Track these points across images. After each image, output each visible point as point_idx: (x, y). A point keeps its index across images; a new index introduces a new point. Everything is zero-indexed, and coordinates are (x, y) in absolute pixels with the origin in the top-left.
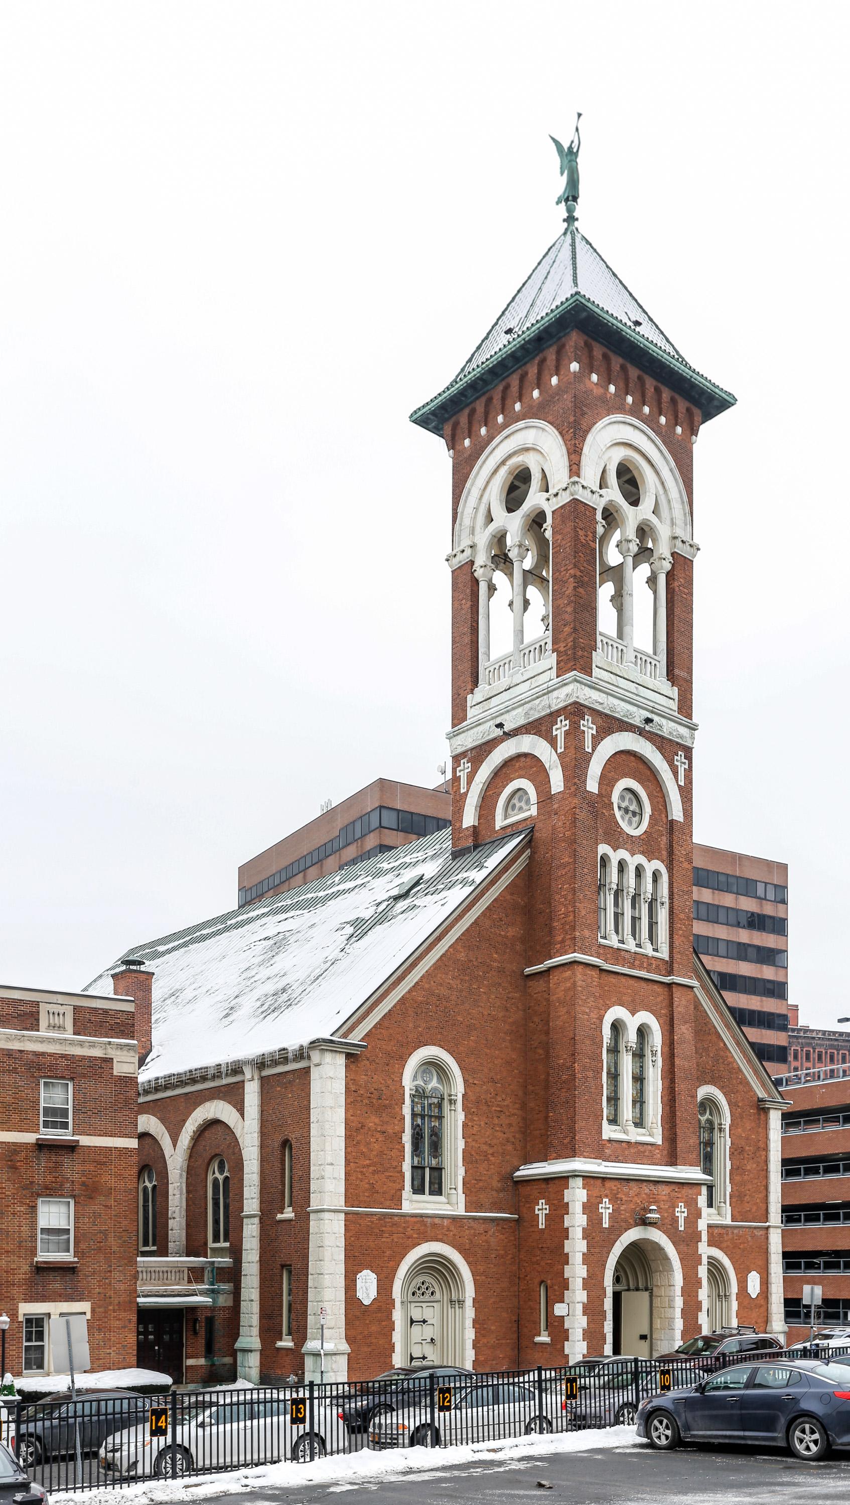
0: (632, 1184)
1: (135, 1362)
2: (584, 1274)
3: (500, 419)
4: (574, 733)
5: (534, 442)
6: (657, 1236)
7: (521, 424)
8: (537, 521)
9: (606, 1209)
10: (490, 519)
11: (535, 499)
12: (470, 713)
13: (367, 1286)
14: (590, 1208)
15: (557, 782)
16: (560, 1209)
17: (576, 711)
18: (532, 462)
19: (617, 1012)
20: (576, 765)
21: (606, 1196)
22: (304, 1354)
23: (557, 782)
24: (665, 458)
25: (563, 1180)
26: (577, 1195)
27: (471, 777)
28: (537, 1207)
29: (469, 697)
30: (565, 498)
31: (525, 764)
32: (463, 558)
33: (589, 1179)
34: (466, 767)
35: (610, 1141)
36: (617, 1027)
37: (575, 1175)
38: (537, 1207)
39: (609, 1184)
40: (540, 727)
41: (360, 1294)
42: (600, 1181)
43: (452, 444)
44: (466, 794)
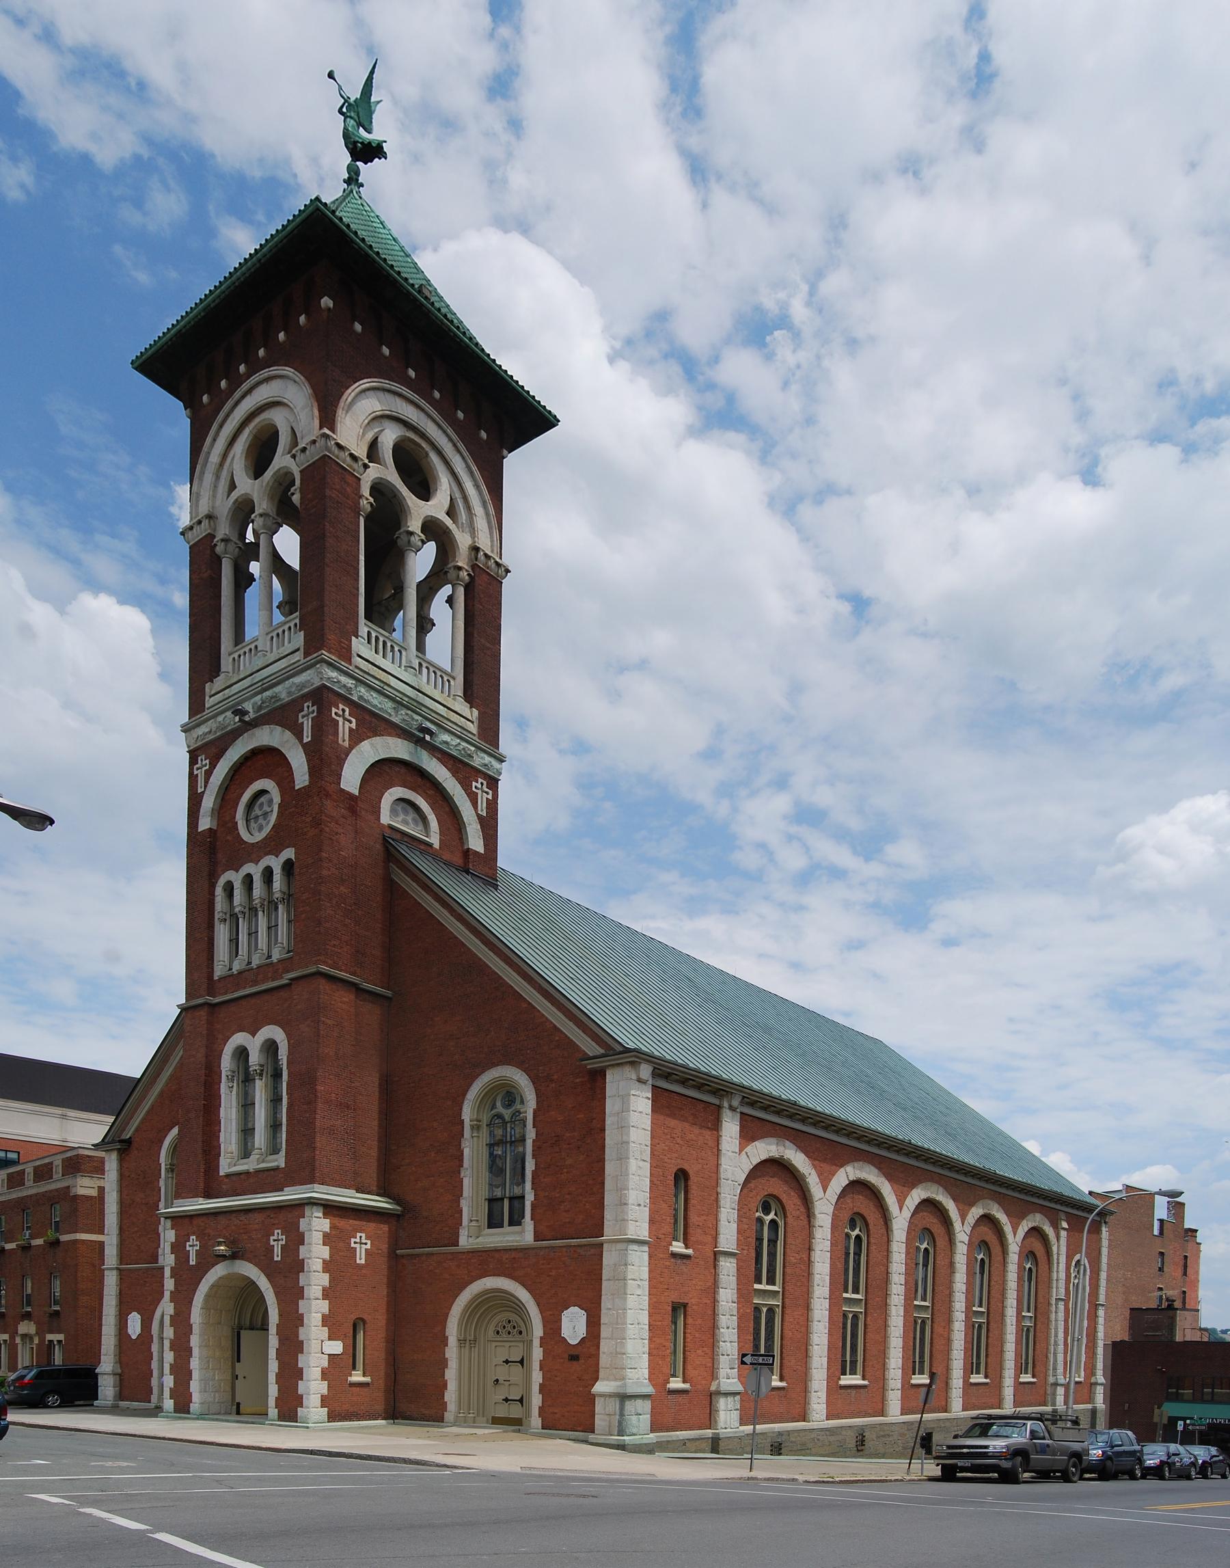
0: (220, 1218)
1: (380, 1407)
2: (172, 1312)
3: (242, 368)
4: (324, 726)
5: (284, 396)
6: (218, 1272)
7: (265, 373)
8: (284, 482)
9: (193, 1246)
10: (232, 486)
11: (281, 461)
12: (209, 702)
13: (134, 1324)
14: (178, 1248)
15: (301, 778)
16: (296, 1239)
17: (322, 696)
18: (278, 417)
19: (239, 1039)
20: (325, 760)
21: (193, 1234)
22: (719, 1393)
23: (301, 778)
24: (423, 410)
25: (299, 1207)
26: (317, 1225)
27: (208, 774)
28: (353, 1240)
29: (208, 685)
30: (312, 455)
31: (267, 761)
32: (199, 533)
33: (330, 1209)
34: (203, 761)
35: (228, 1176)
36: (242, 1054)
37: (312, 1202)
38: (353, 1240)
39: (195, 1221)
40: (283, 715)
41: (130, 1331)
42: (186, 1221)
43: (191, 403)
44: (203, 793)
